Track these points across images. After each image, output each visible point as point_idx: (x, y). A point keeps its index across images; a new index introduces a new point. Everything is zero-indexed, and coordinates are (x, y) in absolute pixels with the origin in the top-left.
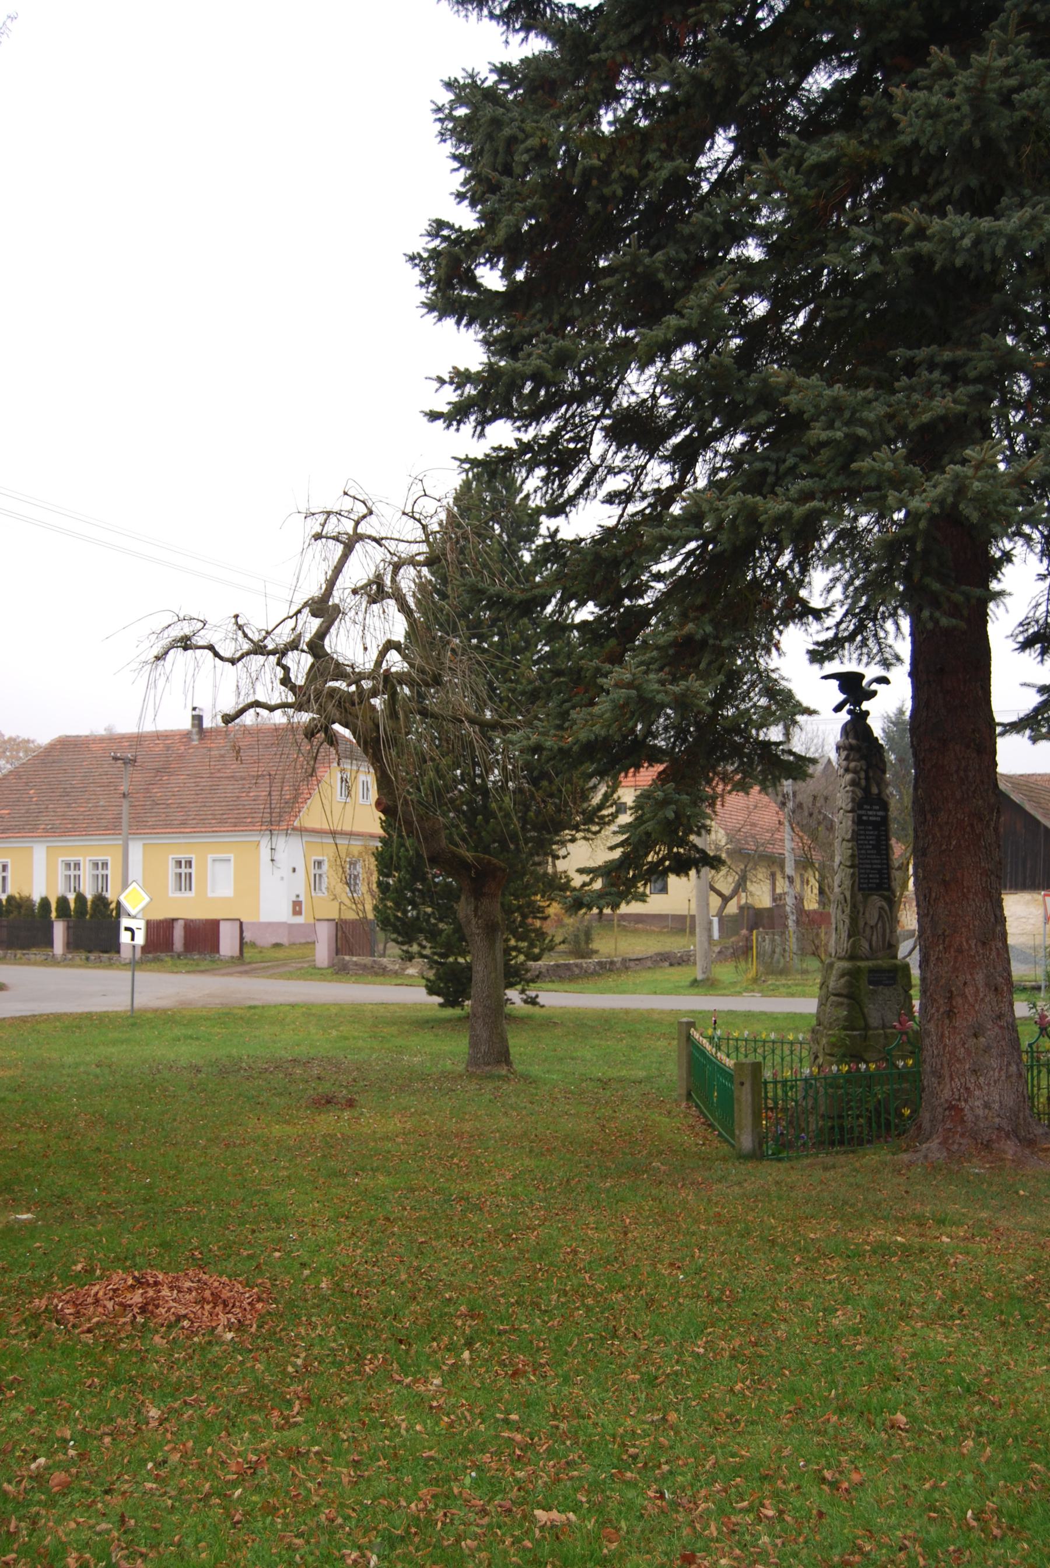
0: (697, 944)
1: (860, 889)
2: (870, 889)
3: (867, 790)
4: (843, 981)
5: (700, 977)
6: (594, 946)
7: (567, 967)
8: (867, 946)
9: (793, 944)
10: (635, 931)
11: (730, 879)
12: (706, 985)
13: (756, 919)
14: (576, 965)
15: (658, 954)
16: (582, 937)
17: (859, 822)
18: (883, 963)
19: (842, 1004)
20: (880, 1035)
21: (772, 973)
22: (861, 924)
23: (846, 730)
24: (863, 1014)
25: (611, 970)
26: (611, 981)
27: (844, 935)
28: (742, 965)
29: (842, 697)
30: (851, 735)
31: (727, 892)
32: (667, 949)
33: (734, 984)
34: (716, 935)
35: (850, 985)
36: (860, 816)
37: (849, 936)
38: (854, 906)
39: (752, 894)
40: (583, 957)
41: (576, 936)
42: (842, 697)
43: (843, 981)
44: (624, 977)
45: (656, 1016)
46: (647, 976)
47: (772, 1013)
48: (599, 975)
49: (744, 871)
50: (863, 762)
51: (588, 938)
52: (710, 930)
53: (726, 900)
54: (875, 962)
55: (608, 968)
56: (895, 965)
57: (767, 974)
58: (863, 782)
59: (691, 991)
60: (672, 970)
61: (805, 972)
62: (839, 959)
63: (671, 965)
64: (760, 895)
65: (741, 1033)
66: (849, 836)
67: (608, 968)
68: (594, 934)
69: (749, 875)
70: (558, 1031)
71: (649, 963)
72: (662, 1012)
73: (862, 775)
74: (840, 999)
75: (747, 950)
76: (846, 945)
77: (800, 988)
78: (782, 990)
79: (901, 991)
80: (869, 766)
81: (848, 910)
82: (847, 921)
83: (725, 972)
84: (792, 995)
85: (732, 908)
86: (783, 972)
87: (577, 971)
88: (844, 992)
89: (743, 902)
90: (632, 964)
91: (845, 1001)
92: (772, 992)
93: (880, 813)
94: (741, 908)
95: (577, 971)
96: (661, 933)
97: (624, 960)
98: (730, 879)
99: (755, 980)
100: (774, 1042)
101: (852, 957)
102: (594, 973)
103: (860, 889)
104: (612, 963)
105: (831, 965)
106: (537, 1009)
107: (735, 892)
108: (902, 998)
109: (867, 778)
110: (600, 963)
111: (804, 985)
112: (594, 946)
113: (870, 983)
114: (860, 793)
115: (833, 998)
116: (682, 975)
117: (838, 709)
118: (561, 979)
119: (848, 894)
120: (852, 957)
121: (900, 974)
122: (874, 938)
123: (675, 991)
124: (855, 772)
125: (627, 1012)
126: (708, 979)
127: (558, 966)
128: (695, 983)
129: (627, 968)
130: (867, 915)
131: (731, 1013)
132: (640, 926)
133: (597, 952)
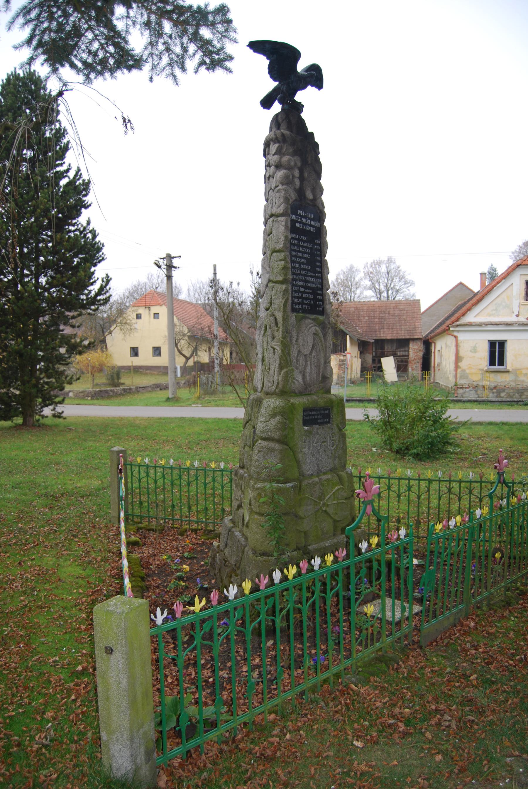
0: (169, 380)
1: (294, 310)
2: (304, 311)
3: (301, 192)
4: (274, 421)
5: (171, 396)
6: (122, 381)
7: (106, 391)
8: (300, 380)
9: (217, 379)
10: (146, 374)
11: (190, 349)
12: (173, 400)
13: (201, 367)
14: (111, 391)
15: (154, 385)
16: (115, 376)
17: (293, 229)
18: (319, 400)
19: (273, 450)
20: (315, 484)
21: (208, 394)
22: (294, 352)
23: (276, 122)
24: (298, 462)
25: (130, 393)
26: (128, 398)
27: (275, 366)
28: (193, 390)
29: (271, 85)
30: (283, 126)
31: (188, 355)
32: (159, 382)
33: (188, 399)
34: (179, 375)
35: (284, 427)
36: (293, 222)
37: (281, 368)
38: (287, 332)
39: (199, 356)
40: (116, 386)
41: (112, 376)
42: (271, 85)
43: (274, 421)
44: (136, 395)
45: (138, 422)
46: (148, 395)
47: (206, 419)
48: (123, 395)
49: (196, 346)
50: (297, 158)
51: (119, 378)
52: (176, 372)
53: (187, 359)
54: (309, 398)
55: (128, 391)
56: (331, 401)
57: (205, 394)
58: (297, 182)
59: (166, 404)
60: (161, 392)
61: (224, 393)
62: (267, 394)
63: (161, 389)
64: (204, 357)
65: (168, 462)
66: (280, 246)
67: (128, 391)
68: (121, 375)
69: (199, 348)
70: (70, 436)
71: (150, 389)
72: (142, 419)
73: (297, 173)
74: (271, 445)
75: (195, 383)
76: (276, 376)
77: (221, 402)
78: (213, 403)
79: (336, 430)
80: (304, 162)
81: (279, 335)
82: (278, 349)
83: (184, 393)
84: (217, 406)
85: (191, 363)
86: (214, 393)
87: (111, 393)
88: (276, 435)
89: (196, 360)
90: (141, 389)
91: (277, 446)
92: (207, 404)
93: (315, 224)
94: (195, 363)
95: (111, 393)
96: (158, 374)
97: (137, 388)
98: (190, 349)
99: (199, 398)
100: (197, 469)
101: (283, 392)
102: (121, 395)
103: (294, 310)
104: (130, 389)
105: (258, 402)
106: (61, 420)
107: (192, 355)
108: (336, 438)
109: (302, 178)
110: (124, 390)
111: (224, 400)
112: (122, 381)
113: (305, 423)
114: (293, 196)
115: (261, 443)
116: (163, 395)
117: (266, 103)
118: (103, 398)
119: (279, 316)
120: (283, 392)
121: (335, 410)
122: (308, 369)
123: (158, 404)
124: (289, 168)
125: (121, 419)
126: (175, 397)
127: (101, 391)
128: (168, 399)
129: (138, 392)
130: (300, 341)
131: (182, 419)
132: (148, 371)
133: (123, 384)
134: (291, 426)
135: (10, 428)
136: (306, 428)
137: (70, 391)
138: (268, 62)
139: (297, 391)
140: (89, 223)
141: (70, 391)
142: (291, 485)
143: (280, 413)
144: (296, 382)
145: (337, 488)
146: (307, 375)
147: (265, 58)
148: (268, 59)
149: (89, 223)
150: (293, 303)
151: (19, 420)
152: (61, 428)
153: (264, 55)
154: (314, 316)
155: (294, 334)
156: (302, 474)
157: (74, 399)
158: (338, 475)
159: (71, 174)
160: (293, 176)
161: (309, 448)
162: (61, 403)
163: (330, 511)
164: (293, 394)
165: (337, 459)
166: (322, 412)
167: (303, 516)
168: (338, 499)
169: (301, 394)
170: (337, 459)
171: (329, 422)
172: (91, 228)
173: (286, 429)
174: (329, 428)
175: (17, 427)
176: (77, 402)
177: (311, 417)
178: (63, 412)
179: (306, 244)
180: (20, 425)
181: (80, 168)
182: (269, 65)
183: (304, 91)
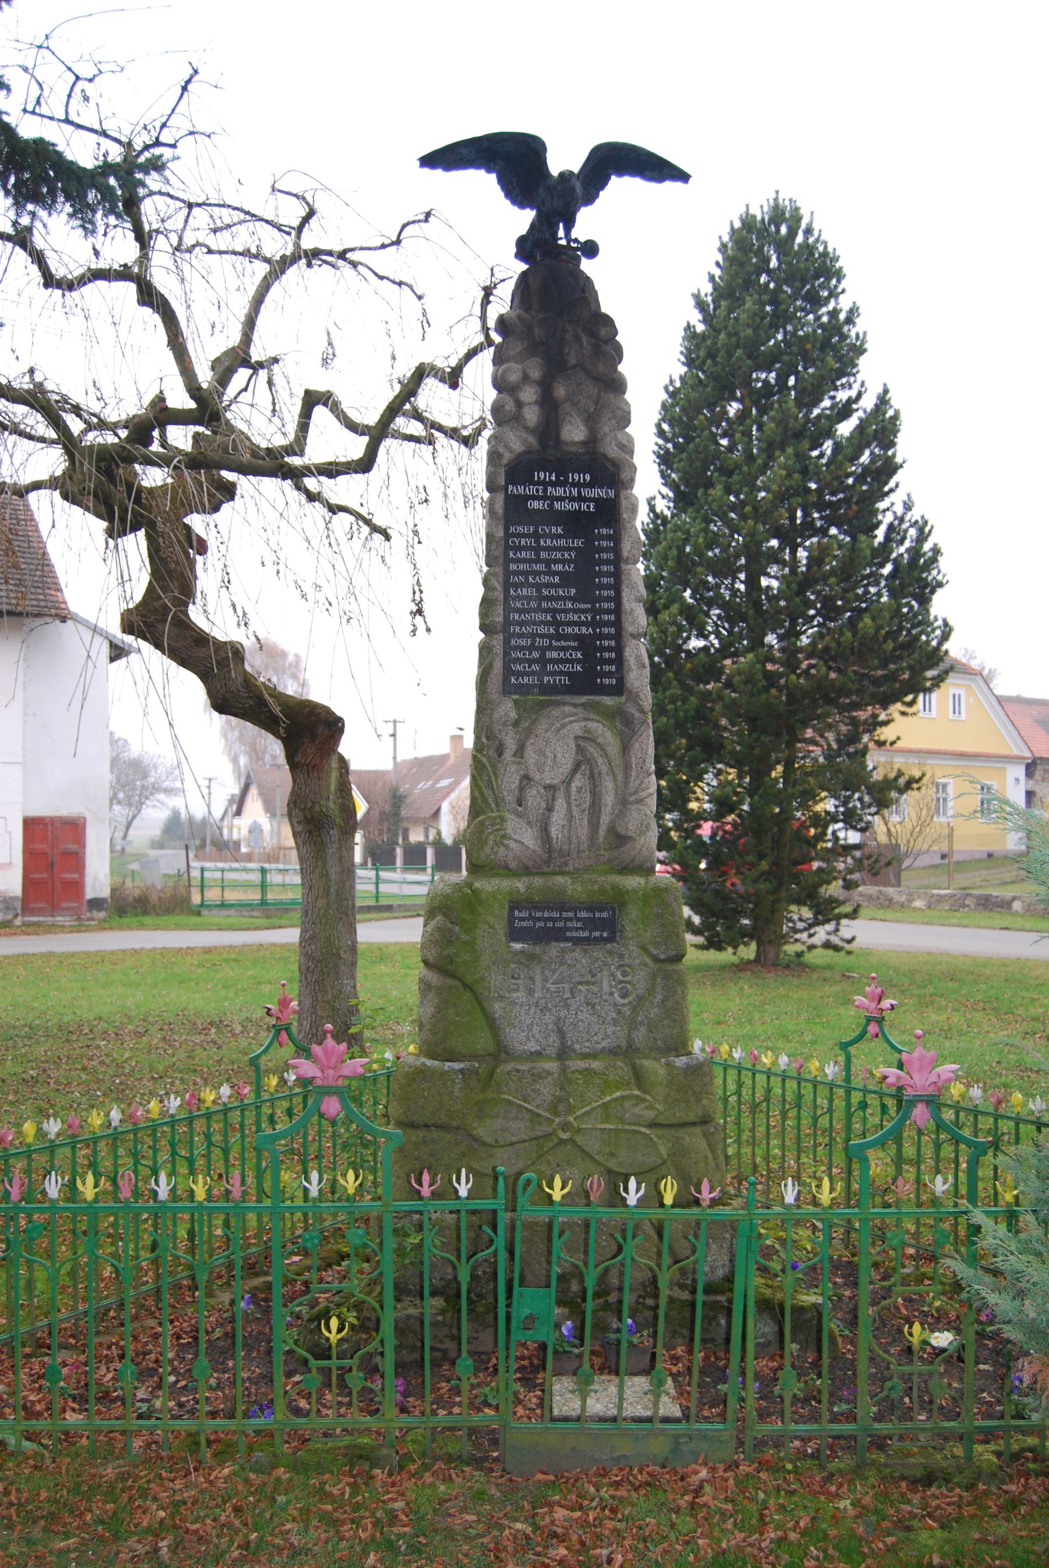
1: (507, 690)
22: (510, 781)
103: (507, 690)
130: (530, 753)
134: (465, 937)
135: (723, 968)
136: (517, 946)
137: (1014, 899)
138: (493, 177)
139: (513, 865)
140: (908, 506)
141: (1014, 899)
142: (457, 1066)
143: (440, 908)
144: (512, 844)
145: (618, 1094)
146: (554, 831)
147: (482, 172)
148: (489, 171)
149: (908, 506)
150: (508, 672)
151: (749, 951)
152: (847, 970)
153: (478, 167)
154: (584, 699)
155: (511, 744)
156: (501, 1052)
157: (1022, 916)
158: (634, 1067)
159: (868, 402)
160: (519, 405)
161: (531, 992)
162: (853, 915)
163: (594, 1146)
164: (504, 872)
165: (643, 1030)
166: (584, 914)
167: (489, 1140)
168: (621, 1120)
169: (526, 871)
170: (643, 1030)
171: (611, 939)
172: (915, 515)
173: (450, 943)
174: (610, 952)
175: (743, 967)
176: (1029, 925)
177: (539, 924)
178: (853, 939)
179: (562, 542)
180: (749, 962)
181: (889, 386)
182: (500, 182)
183: (653, 186)
